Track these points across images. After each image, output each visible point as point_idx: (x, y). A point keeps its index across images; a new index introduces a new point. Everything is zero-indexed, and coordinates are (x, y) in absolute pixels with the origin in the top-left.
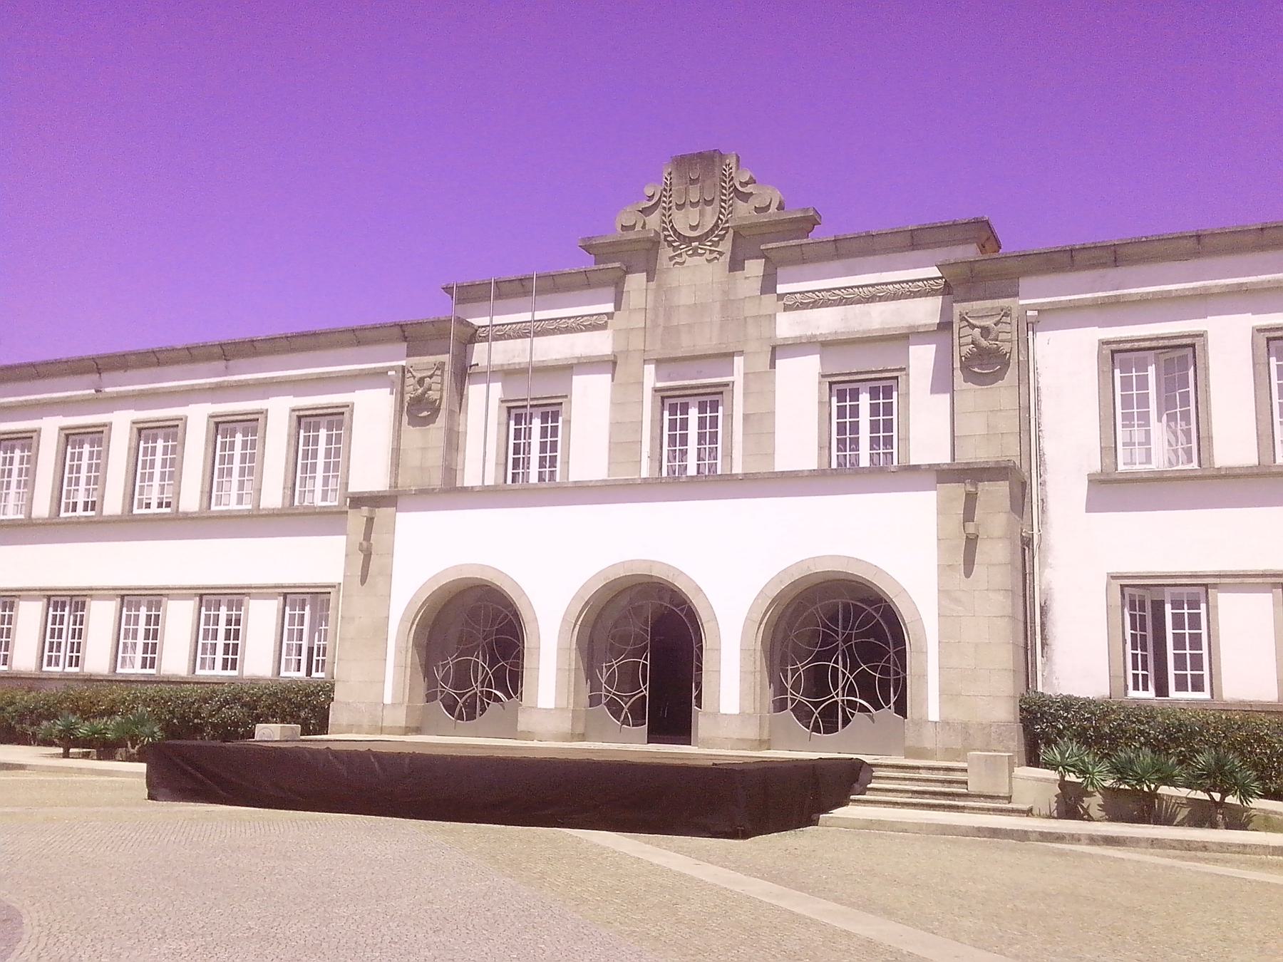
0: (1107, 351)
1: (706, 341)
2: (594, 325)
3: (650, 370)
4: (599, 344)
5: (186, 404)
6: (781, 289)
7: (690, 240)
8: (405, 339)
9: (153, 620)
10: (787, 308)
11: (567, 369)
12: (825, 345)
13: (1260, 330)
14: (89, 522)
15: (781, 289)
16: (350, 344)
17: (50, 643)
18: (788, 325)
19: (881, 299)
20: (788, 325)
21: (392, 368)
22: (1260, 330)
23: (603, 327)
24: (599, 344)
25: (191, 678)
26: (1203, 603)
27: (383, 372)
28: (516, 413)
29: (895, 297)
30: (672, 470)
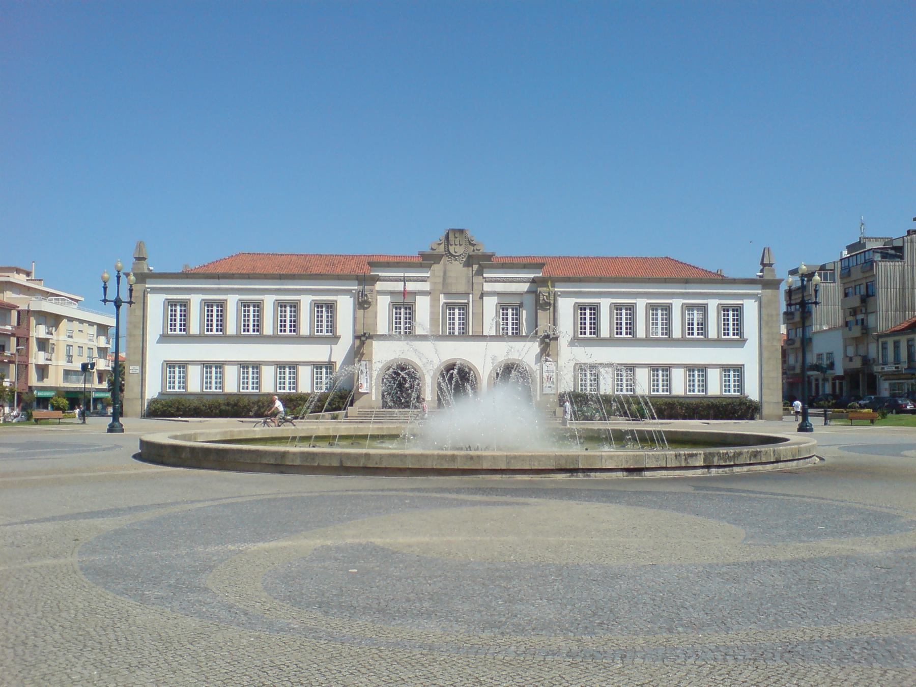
0: (577, 305)
1: (462, 288)
2: (423, 280)
3: (442, 296)
4: (426, 286)
5: (264, 295)
6: (485, 275)
7: (455, 256)
8: (357, 279)
9: (296, 373)
10: (486, 282)
11: (414, 294)
12: (392, 293)
13: (167, 299)
14: (182, 336)
15: (485, 275)
16: (184, 278)
17: (242, 380)
18: (487, 287)
19: (514, 282)
20: (487, 287)
21: (354, 290)
22: (203, 300)
23: (426, 281)
24: (426, 286)
25: (685, 395)
26: (6, 406)
27: (351, 290)
28: (396, 306)
29: (519, 282)
30: (450, 333)
